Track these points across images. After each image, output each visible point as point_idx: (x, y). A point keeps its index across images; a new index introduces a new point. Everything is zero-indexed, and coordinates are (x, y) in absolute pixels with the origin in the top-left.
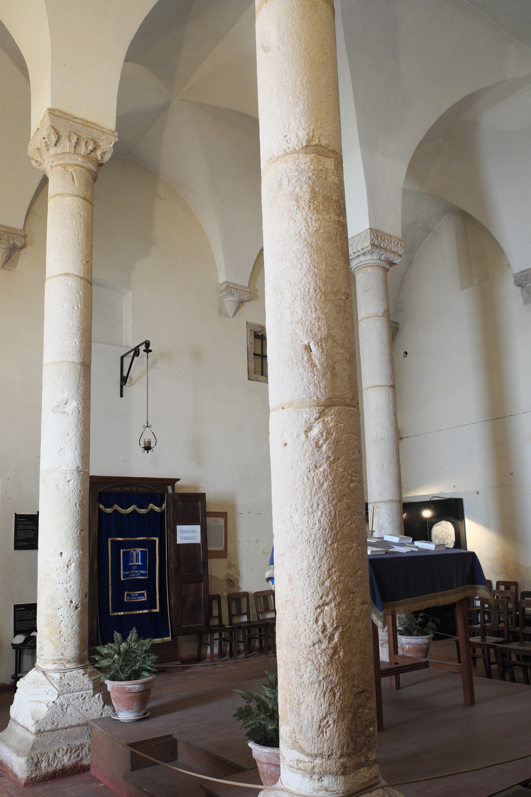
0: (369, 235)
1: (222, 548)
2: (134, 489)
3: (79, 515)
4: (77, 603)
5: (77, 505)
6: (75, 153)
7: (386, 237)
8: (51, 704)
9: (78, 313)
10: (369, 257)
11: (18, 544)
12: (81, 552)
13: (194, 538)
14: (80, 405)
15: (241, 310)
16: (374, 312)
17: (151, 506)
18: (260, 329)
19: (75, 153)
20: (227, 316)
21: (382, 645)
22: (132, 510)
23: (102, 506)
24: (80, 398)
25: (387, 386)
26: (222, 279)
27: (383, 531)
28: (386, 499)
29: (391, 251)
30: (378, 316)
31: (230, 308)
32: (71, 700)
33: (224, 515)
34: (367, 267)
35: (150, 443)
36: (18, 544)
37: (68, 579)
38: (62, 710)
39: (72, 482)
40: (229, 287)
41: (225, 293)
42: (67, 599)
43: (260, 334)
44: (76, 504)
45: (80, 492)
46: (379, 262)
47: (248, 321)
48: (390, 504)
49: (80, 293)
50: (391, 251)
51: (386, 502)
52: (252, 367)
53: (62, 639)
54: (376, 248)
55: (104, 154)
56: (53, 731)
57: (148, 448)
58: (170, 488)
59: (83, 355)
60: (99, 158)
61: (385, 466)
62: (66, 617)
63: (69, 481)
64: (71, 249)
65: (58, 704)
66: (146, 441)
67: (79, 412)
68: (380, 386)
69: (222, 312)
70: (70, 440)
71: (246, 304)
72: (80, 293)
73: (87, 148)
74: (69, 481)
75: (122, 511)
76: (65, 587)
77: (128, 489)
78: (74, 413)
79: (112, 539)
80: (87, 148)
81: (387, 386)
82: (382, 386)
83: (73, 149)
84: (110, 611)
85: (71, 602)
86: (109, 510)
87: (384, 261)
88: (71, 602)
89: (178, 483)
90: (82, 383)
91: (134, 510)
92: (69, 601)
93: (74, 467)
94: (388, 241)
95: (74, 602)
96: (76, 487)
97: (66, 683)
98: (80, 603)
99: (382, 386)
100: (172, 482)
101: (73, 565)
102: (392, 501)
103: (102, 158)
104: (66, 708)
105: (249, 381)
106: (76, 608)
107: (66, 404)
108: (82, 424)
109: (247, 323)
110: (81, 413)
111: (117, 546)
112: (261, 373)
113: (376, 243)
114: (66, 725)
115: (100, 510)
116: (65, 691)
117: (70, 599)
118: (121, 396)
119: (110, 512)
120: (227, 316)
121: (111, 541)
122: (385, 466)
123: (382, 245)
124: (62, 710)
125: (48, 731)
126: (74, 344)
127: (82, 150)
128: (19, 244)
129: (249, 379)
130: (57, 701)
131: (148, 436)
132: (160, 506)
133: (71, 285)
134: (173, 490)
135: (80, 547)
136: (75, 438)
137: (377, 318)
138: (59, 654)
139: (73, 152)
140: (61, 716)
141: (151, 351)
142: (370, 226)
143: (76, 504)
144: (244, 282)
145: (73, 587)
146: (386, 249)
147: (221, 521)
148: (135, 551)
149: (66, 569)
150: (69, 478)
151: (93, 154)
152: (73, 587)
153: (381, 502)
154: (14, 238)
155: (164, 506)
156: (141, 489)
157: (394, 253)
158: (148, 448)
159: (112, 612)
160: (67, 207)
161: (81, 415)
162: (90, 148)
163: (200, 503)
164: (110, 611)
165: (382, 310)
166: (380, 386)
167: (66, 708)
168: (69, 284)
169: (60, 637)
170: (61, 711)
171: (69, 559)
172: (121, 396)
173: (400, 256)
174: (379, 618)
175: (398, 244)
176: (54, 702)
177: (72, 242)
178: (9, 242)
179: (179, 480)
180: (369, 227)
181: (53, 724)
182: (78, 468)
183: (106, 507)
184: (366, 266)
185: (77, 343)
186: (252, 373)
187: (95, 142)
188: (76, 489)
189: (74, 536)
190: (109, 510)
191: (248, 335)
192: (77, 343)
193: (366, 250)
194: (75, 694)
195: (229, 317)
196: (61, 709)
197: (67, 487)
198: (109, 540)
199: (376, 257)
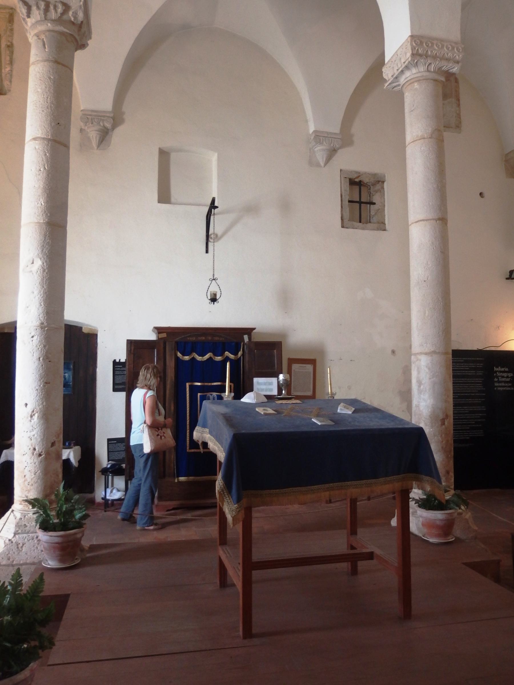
0: (409, 43)
1: (310, 393)
2: (210, 338)
3: (42, 368)
4: (40, 451)
5: (41, 359)
6: (46, 19)
7: (435, 42)
8: (7, 541)
9: (45, 175)
10: (414, 71)
11: (116, 387)
12: (44, 404)
13: (271, 390)
14: (45, 264)
15: (334, 158)
16: (420, 134)
17: (227, 353)
18: (356, 176)
19: (46, 19)
20: (318, 165)
21: (413, 514)
22: (208, 357)
23: (179, 355)
24: (45, 257)
25: (433, 219)
26: (312, 128)
27: (422, 387)
28: (427, 350)
29: (443, 58)
30: (424, 138)
31: (320, 156)
32: (26, 540)
33: (313, 362)
34: (413, 82)
35: (215, 295)
36: (116, 387)
37: (31, 428)
38: (18, 548)
39: (35, 338)
40: (319, 137)
41: (314, 143)
42: (30, 447)
43: (357, 180)
44: (39, 358)
45: (45, 346)
46: (427, 74)
47: (342, 168)
48: (432, 356)
49: (48, 154)
50: (443, 58)
51: (426, 354)
52: (347, 215)
53: (26, 483)
54: (418, 57)
55: (75, 14)
56: (8, 565)
57: (214, 300)
58: (246, 337)
59: (49, 215)
60: (72, 19)
61: (427, 312)
62: (29, 463)
63: (33, 337)
64: (40, 113)
65: (14, 542)
66: (212, 292)
67: (44, 271)
68: (421, 221)
69: (312, 163)
70: (35, 298)
71: (340, 151)
72: (48, 154)
73: (56, 11)
74: (33, 337)
75: (199, 358)
76: (28, 436)
77: (204, 338)
78: (39, 272)
79: (190, 383)
80: (56, 11)
81: (433, 219)
82: (427, 220)
83: (43, 16)
84: (188, 448)
85: (35, 449)
86: (187, 358)
87: (434, 72)
88: (35, 449)
89: (254, 331)
90: (48, 243)
91: (210, 358)
92: (32, 449)
93: (38, 323)
94: (438, 47)
95: (37, 450)
96: (39, 341)
97: (23, 523)
98: (43, 451)
99: (427, 220)
100: (249, 331)
101: (36, 415)
102: (434, 352)
103: (75, 18)
104: (22, 547)
105: (343, 229)
106: (40, 455)
107: (33, 263)
108: (47, 282)
109: (341, 170)
110: (46, 271)
111: (194, 390)
112: (359, 221)
113: (420, 51)
114: (21, 562)
115: (177, 358)
116: (20, 531)
117: (33, 446)
118: (207, 252)
119: (198, 359)
120: (318, 165)
121: (190, 386)
122: (427, 312)
123: (429, 53)
124: (18, 548)
125: (4, 565)
126: (39, 205)
127: (53, 15)
128: (108, 125)
129: (343, 227)
130: (13, 540)
131: (214, 288)
132: (236, 354)
133: (39, 149)
134: (250, 338)
135: (44, 399)
136: (39, 296)
137: (422, 141)
138: (24, 496)
139: (43, 19)
140: (16, 553)
141: (217, 207)
142: (412, 32)
143: (39, 358)
144: (335, 128)
145: (36, 436)
146: (435, 57)
147: (309, 368)
148: (211, 395)
149: (29, 418)
150: (32, 334)
151: (65, 17)
152: (36, 436)
153: (421, 353)
154: (103, 120)
155: (240, 353)
156: (217, 339)
157: (448, 60)
158: (214, 300)
159: (190, 449)
160: (38, 74)
161: (47, 273)
162: (60, 10)
163: (275, 351)
164: (188, 448)
165: (430, 130)
166: (421, 221)
167: (22, 547)
168: (37, 147)
169: (25, 481)
170: (17, 549)
171: (32, 410)
172: (207, 252)
173: (458, 62)
174: (231, 511)
175: (453, 48)
176: (10, 540)
177: (41, 106)
178: (100, 125)
179: (254, 329)
180: (410, 34)
181: (9, 559)
182: (42, 323)
183: (184, 355)
184: (410, 82)
185: (43, 204)
186: (346, 221)
187: (64, 4)
188: (39, 344)
189: (37, 388)
190: (187, 358)
191: (343, 182)
192: (43, 204)
193: (407, 62)
194: (31, 535)
195: (321, 167)
196: (16, 547)
197: (31, 342)
198: (188, 385)
199: (422, 68)
